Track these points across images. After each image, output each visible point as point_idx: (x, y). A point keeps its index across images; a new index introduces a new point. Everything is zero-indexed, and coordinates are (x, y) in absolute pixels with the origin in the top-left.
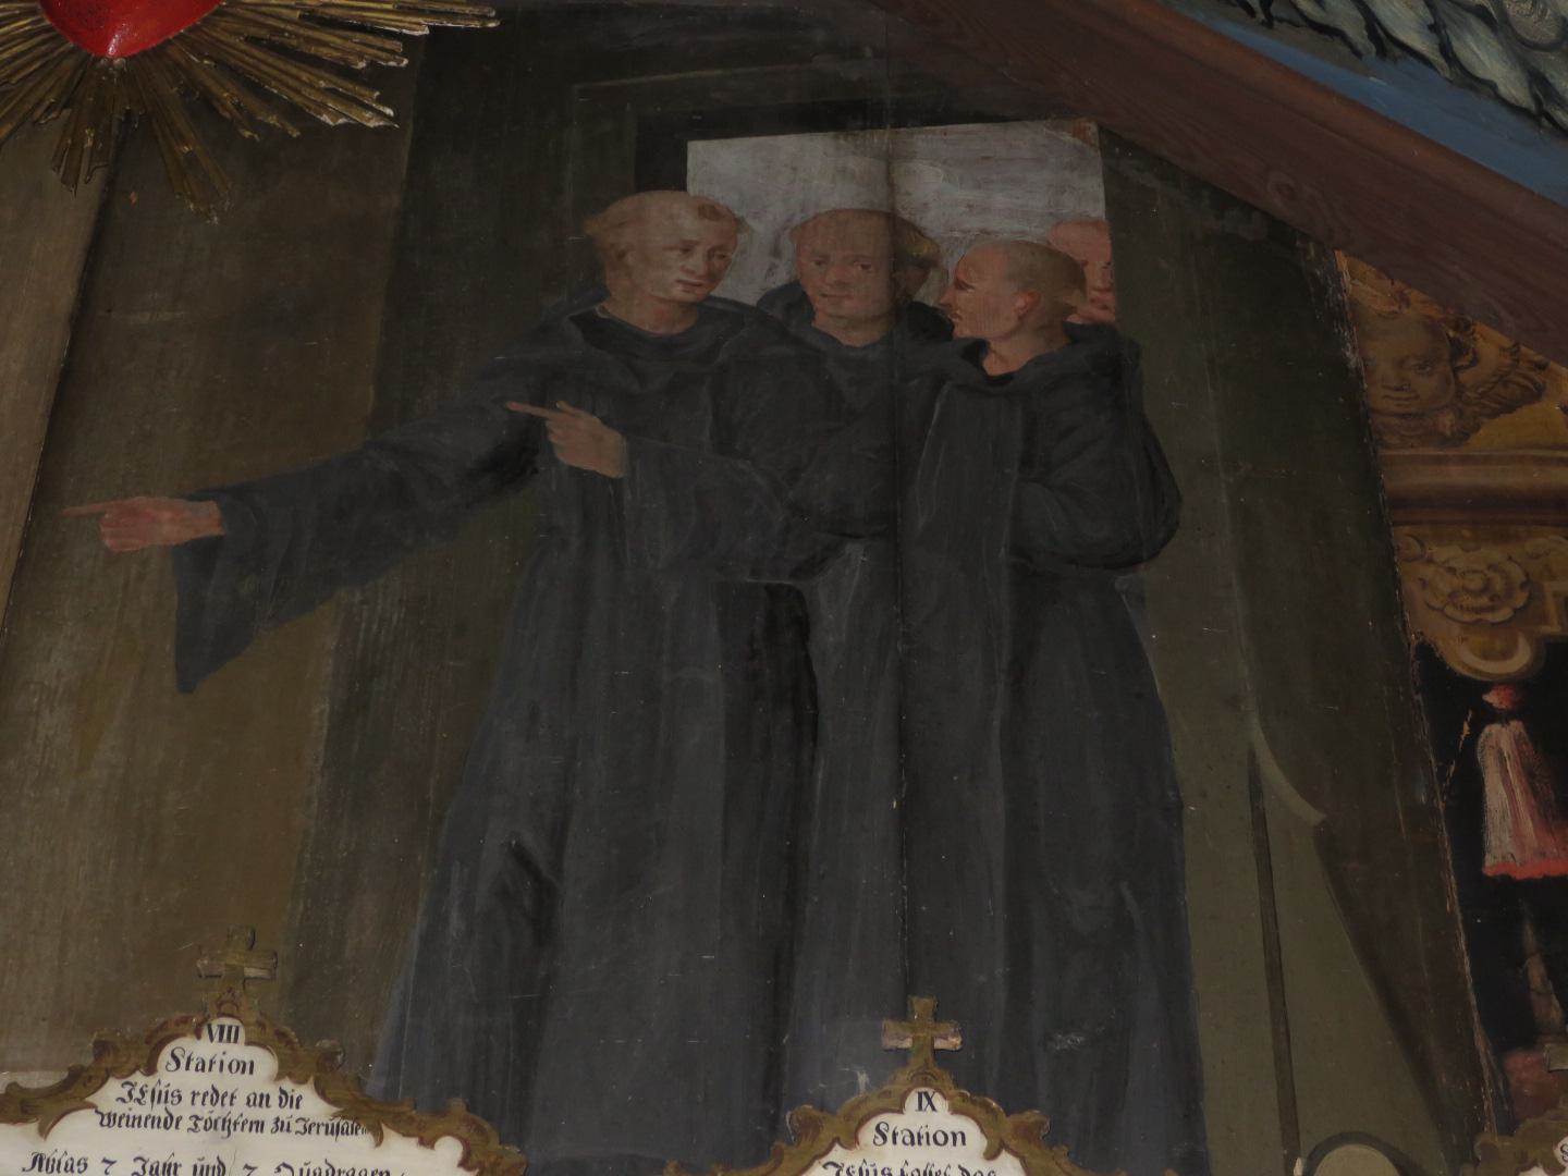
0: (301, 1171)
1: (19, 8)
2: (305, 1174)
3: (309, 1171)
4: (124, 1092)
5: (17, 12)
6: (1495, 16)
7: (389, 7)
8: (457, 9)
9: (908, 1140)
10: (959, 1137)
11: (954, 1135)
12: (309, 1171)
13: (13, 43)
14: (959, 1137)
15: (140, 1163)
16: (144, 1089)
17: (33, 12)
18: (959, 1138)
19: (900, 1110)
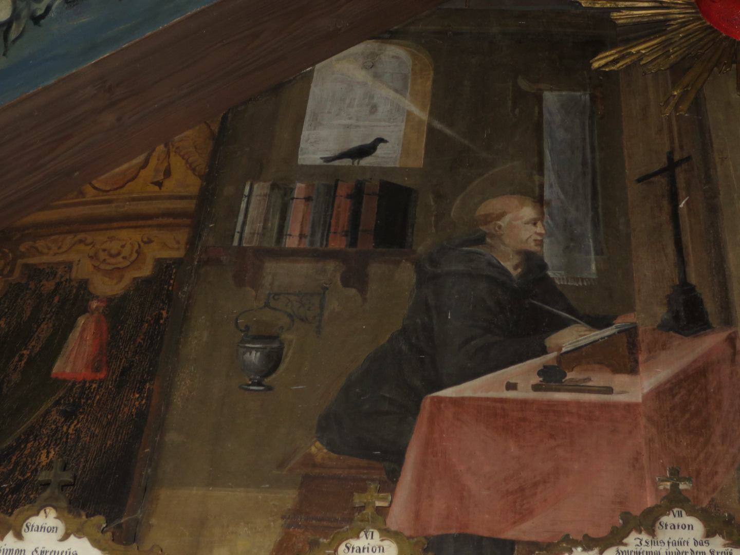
0: (66, 552)
1: (693, 17)
2: (68, 554)
3: (70, 552)
4: (638, 542)
5: (691, 19)
6: (464, 248)
7: (537, 109)
8: (238, 229)
9: (672, 527)
10: (691, 527)
11: (689, 526)
12: (70, 552)
13: (571, 387)
14: (691, 527)
15: (639, 541)
16: (647, 541)
17: (699, 19)
18: (690, 527)
19: (358, 537)
